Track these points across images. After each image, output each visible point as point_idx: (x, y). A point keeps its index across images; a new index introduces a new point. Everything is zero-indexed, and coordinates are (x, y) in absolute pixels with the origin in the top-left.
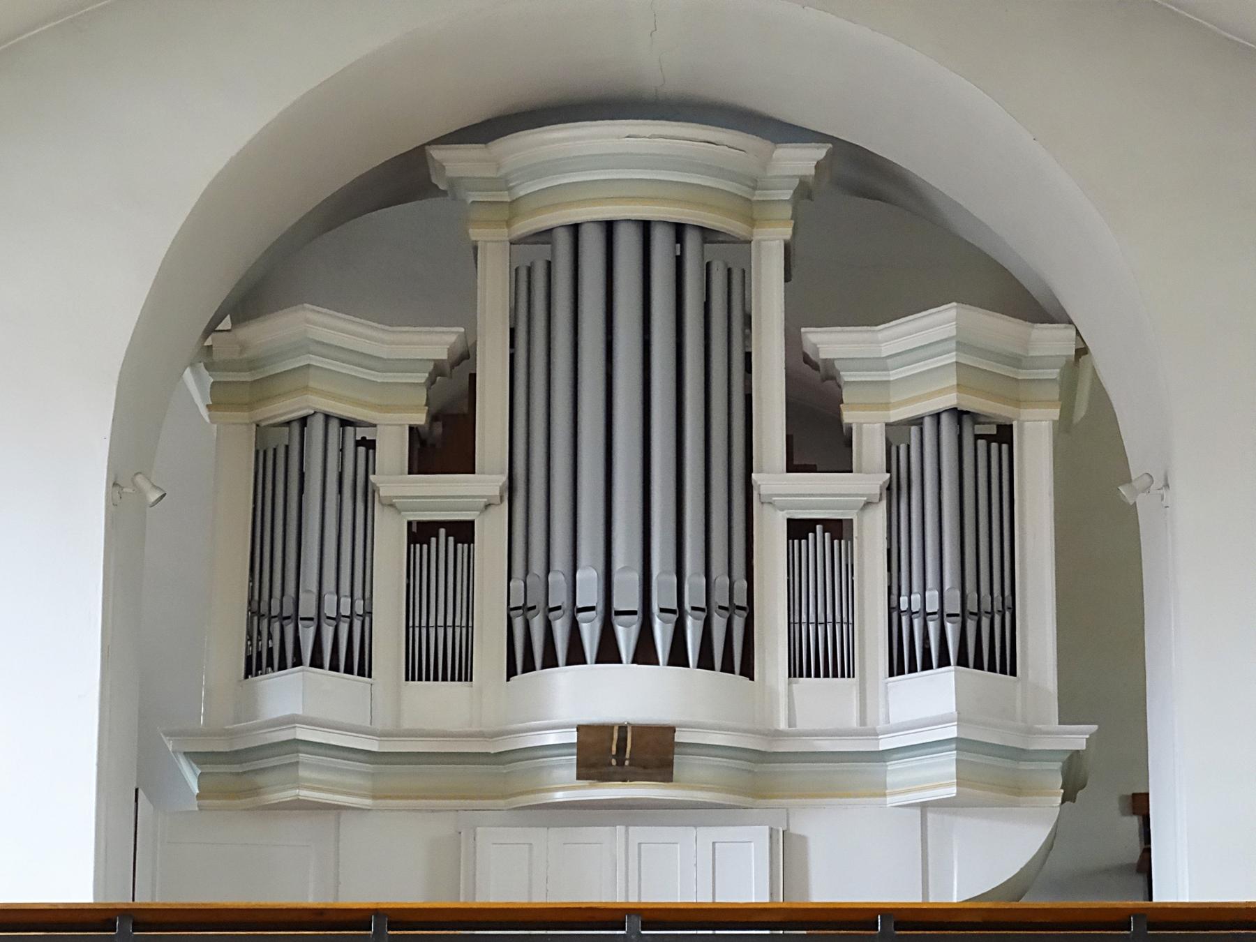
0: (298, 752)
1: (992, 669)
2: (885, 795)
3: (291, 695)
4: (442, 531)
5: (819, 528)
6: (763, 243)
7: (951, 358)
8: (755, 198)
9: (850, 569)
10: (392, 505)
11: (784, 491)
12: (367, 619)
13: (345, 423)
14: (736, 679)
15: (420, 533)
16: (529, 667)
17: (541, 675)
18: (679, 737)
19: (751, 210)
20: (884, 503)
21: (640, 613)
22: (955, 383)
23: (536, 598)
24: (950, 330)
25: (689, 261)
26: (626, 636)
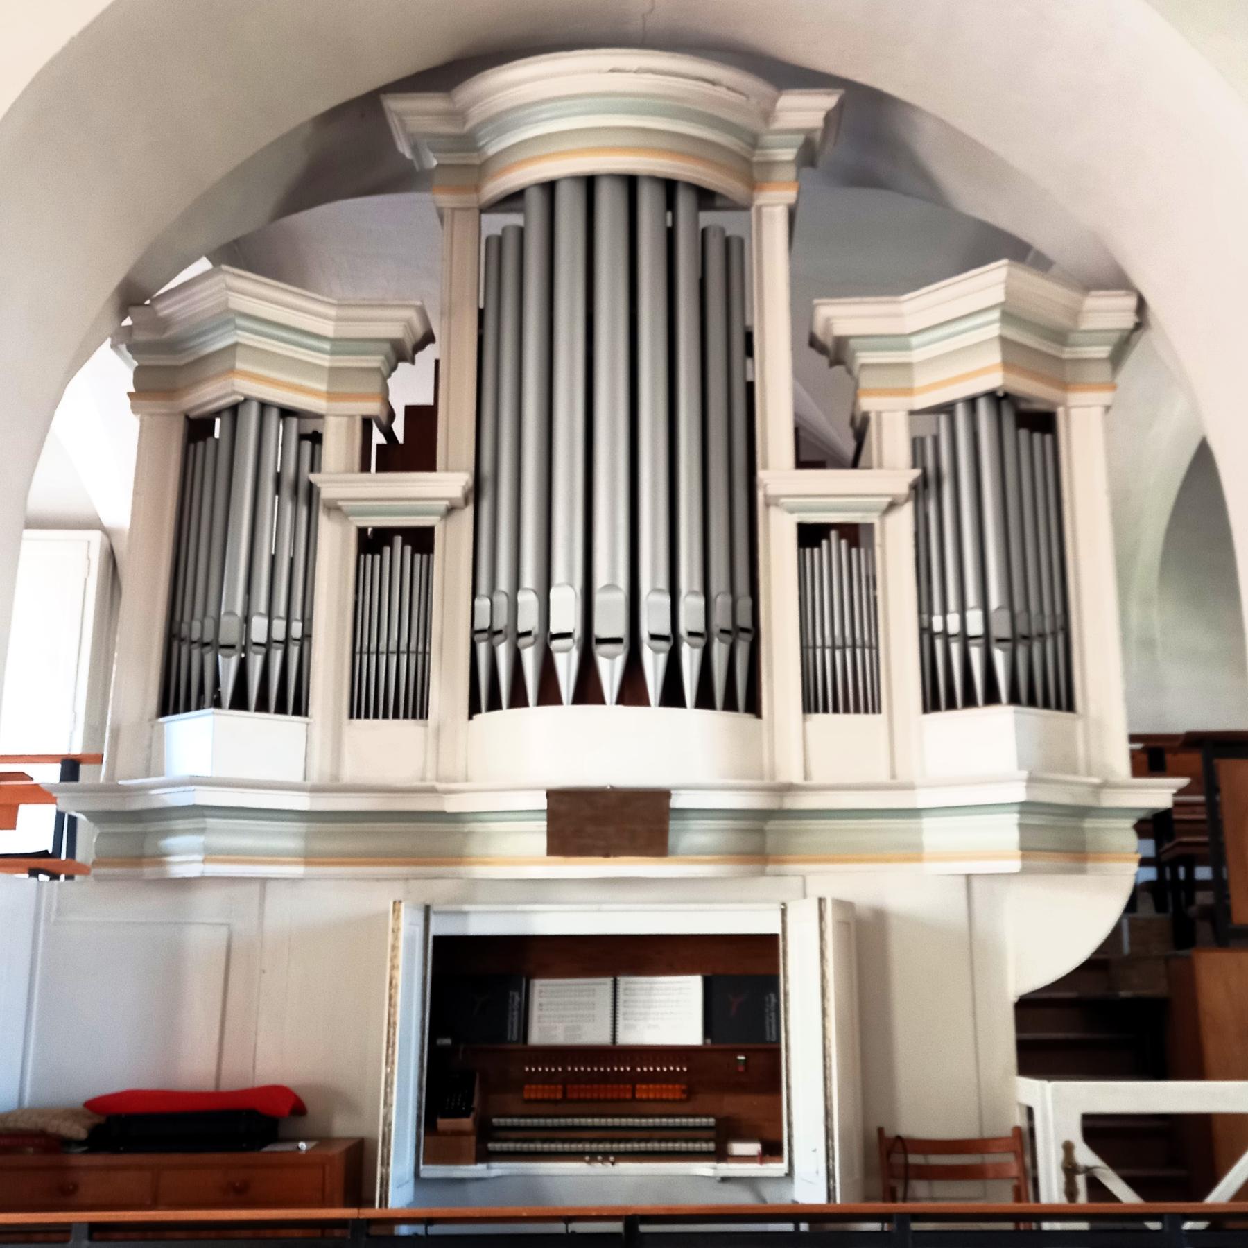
0: (205, 816)
1: (1046, 705)
3: (205, 747)
4: (398, 540)
5: (833, 534)
6: (765, 210)
8: (755, 159)
9: (872, 582)
10: (338, 509)
11: (791, 492)
12: (306, 644)
13: (286, 413)
14: (740, 719)
15: (372, 542)
16: (494, 704)
17: (506, 716)
18: (677, 802)
19: (754, 172)
20: (469, 512)
21: (626, 641)
23: (954, 626)
24: (998, 296)
25: (679, 228)
26: (610, 669)
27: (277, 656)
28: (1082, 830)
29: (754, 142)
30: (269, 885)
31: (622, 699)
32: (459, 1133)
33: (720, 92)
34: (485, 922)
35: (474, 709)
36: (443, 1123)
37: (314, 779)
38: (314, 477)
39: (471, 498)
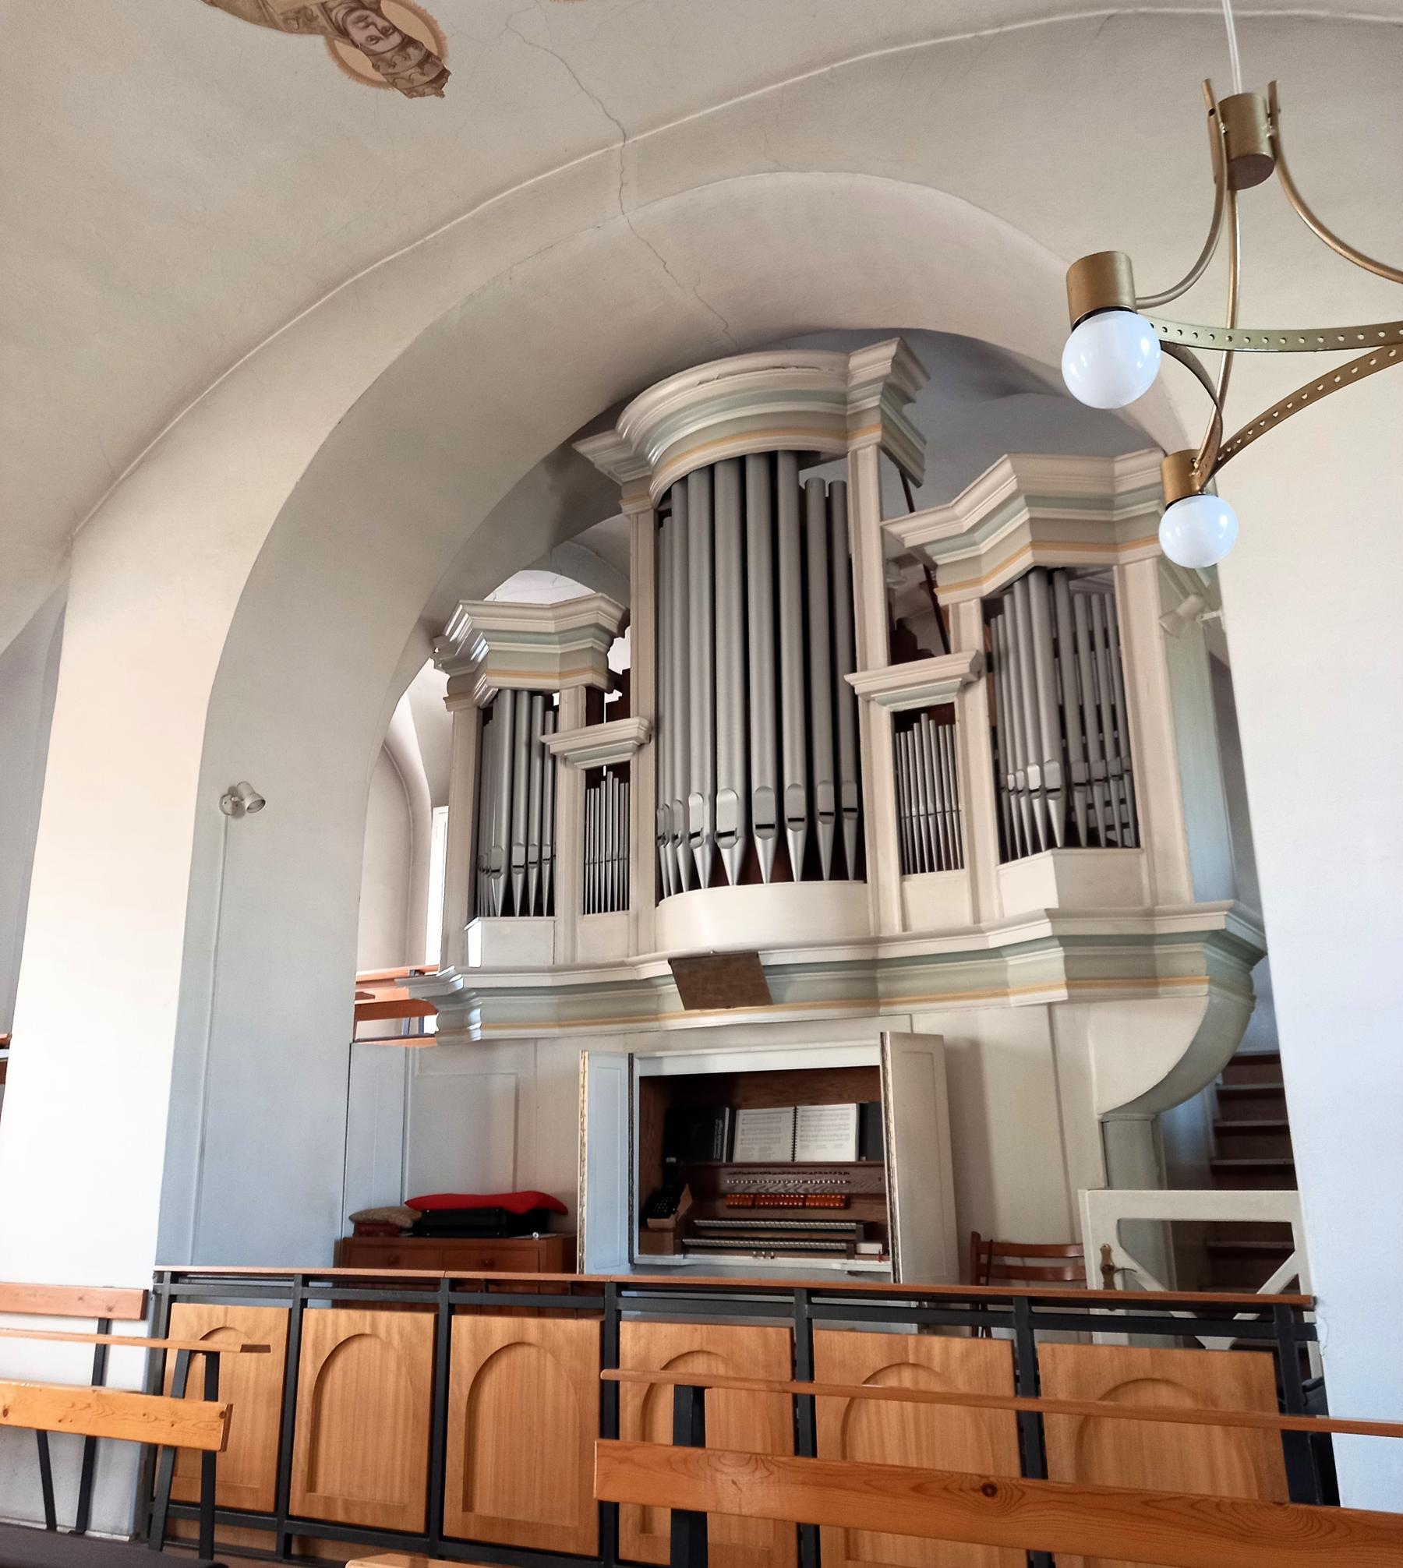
2: (1006, 995)
5: (923, 716)
7: (1024, 516)
11: (881, 682)
14: (850, 886)
19: (843, 423)
22: (1029, 539)
23: (699, 820)
26: (732, 859)
28: (1153, 957)
29: (843, 400)
30: (540, 1043)
31: (774, 879)
32: (663, 1230)
33: (791, 372)
34: (674, 1066)
35: (660, 896)
36: (652, 1222)
37: (561, 961)
38: (849, 678)
39: (653, 734)
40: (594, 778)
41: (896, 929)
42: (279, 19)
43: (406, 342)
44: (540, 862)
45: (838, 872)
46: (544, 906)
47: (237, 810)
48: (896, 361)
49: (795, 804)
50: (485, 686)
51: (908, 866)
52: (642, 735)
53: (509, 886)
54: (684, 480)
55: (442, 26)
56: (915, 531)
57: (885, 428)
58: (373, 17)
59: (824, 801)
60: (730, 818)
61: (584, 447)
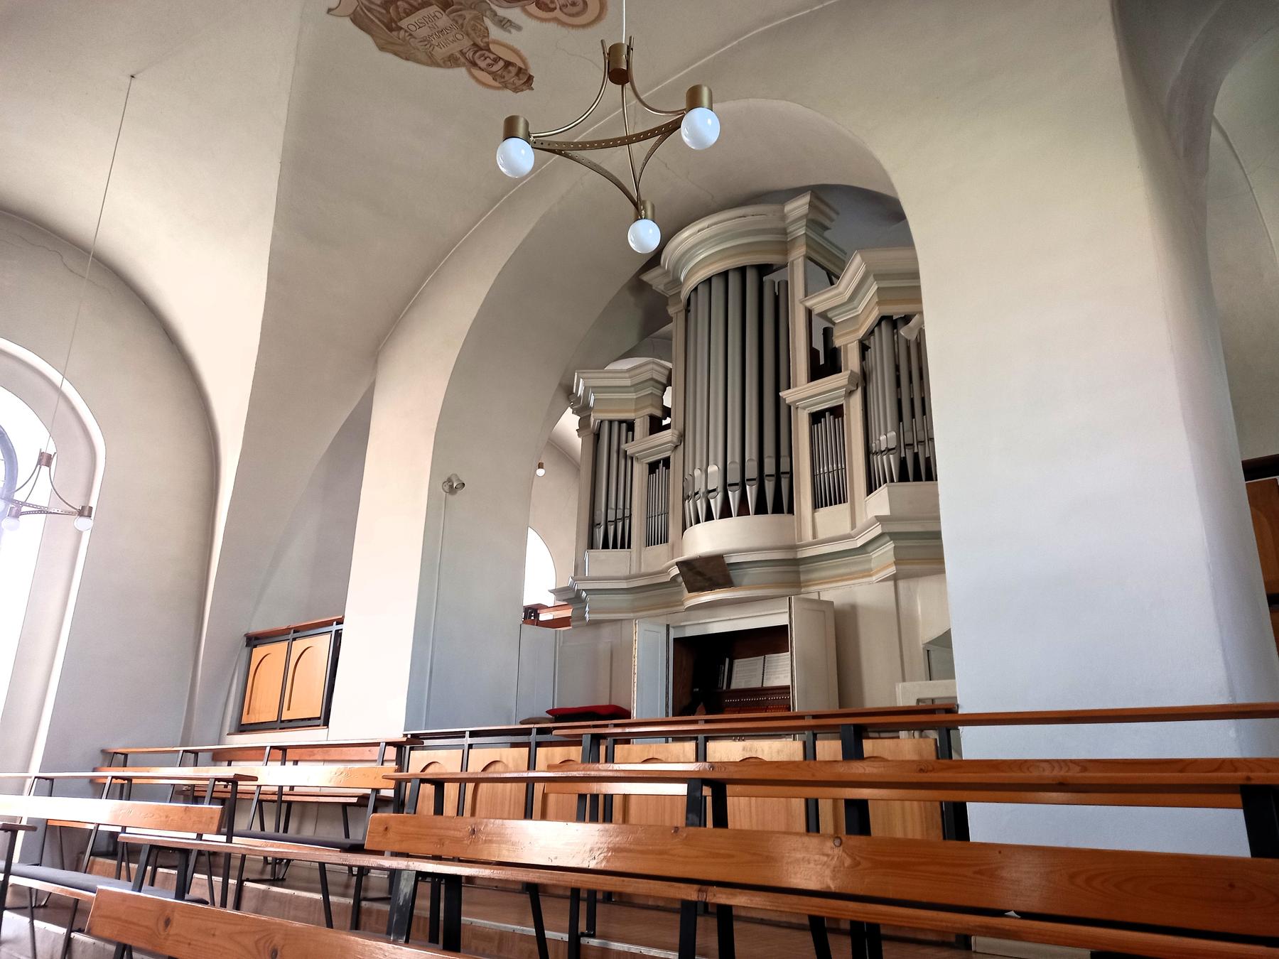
7: (874, 288)
11: (804, 394)
14: (784, 518)
19: (785, 246)
27: (620, 525)
29: (784, 232)
34: (690, 632)
37: (633, 572)
40: (653, 467)
41: (808, 537)
42: (441, 62)
43: (531, 226)
44: (623, 519)
45: (778, 509)
46: (625, 543)
47: (452, 490)
48: (811, 204)
49: (751, 471)
50: (594, 418)
51: (817, 505)
52: (675, 439)
53: (605, 532)
54: (696, 289)
55: (524, 53)
56: (820, 302)
57: (808, 246)
58: (487, 54)
59: (769, 467)
60: (715, 482)
61: (647, 277)
